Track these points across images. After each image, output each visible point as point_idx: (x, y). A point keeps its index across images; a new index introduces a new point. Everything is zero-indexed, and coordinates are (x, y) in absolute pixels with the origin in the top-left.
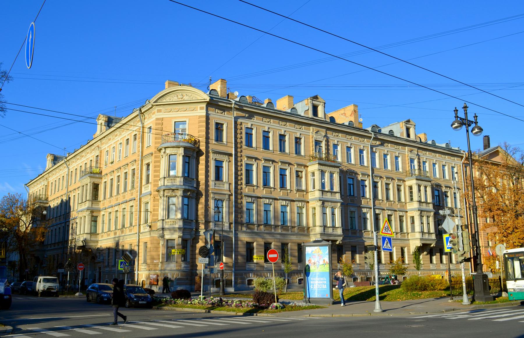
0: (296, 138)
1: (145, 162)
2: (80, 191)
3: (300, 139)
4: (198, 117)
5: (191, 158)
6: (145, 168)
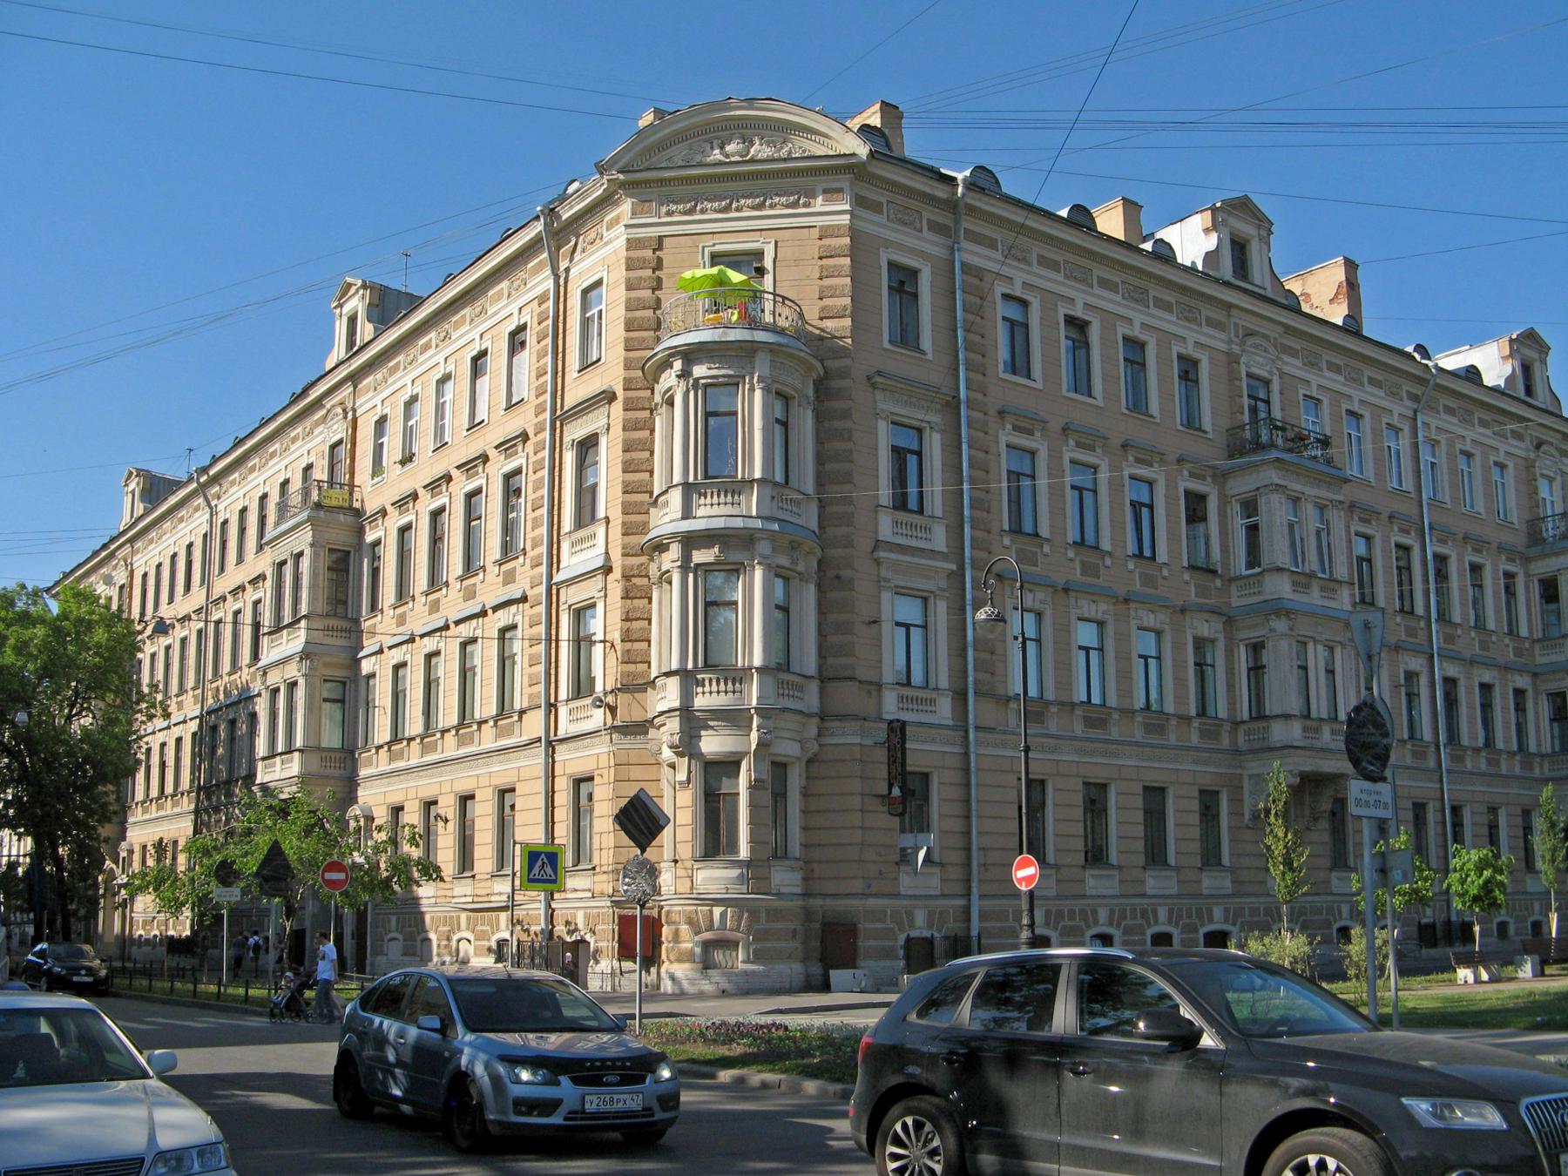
1: (576, 431)
2: (266, 592)
4: (815, 233)
5: (794, 404)
6: (569, 458)
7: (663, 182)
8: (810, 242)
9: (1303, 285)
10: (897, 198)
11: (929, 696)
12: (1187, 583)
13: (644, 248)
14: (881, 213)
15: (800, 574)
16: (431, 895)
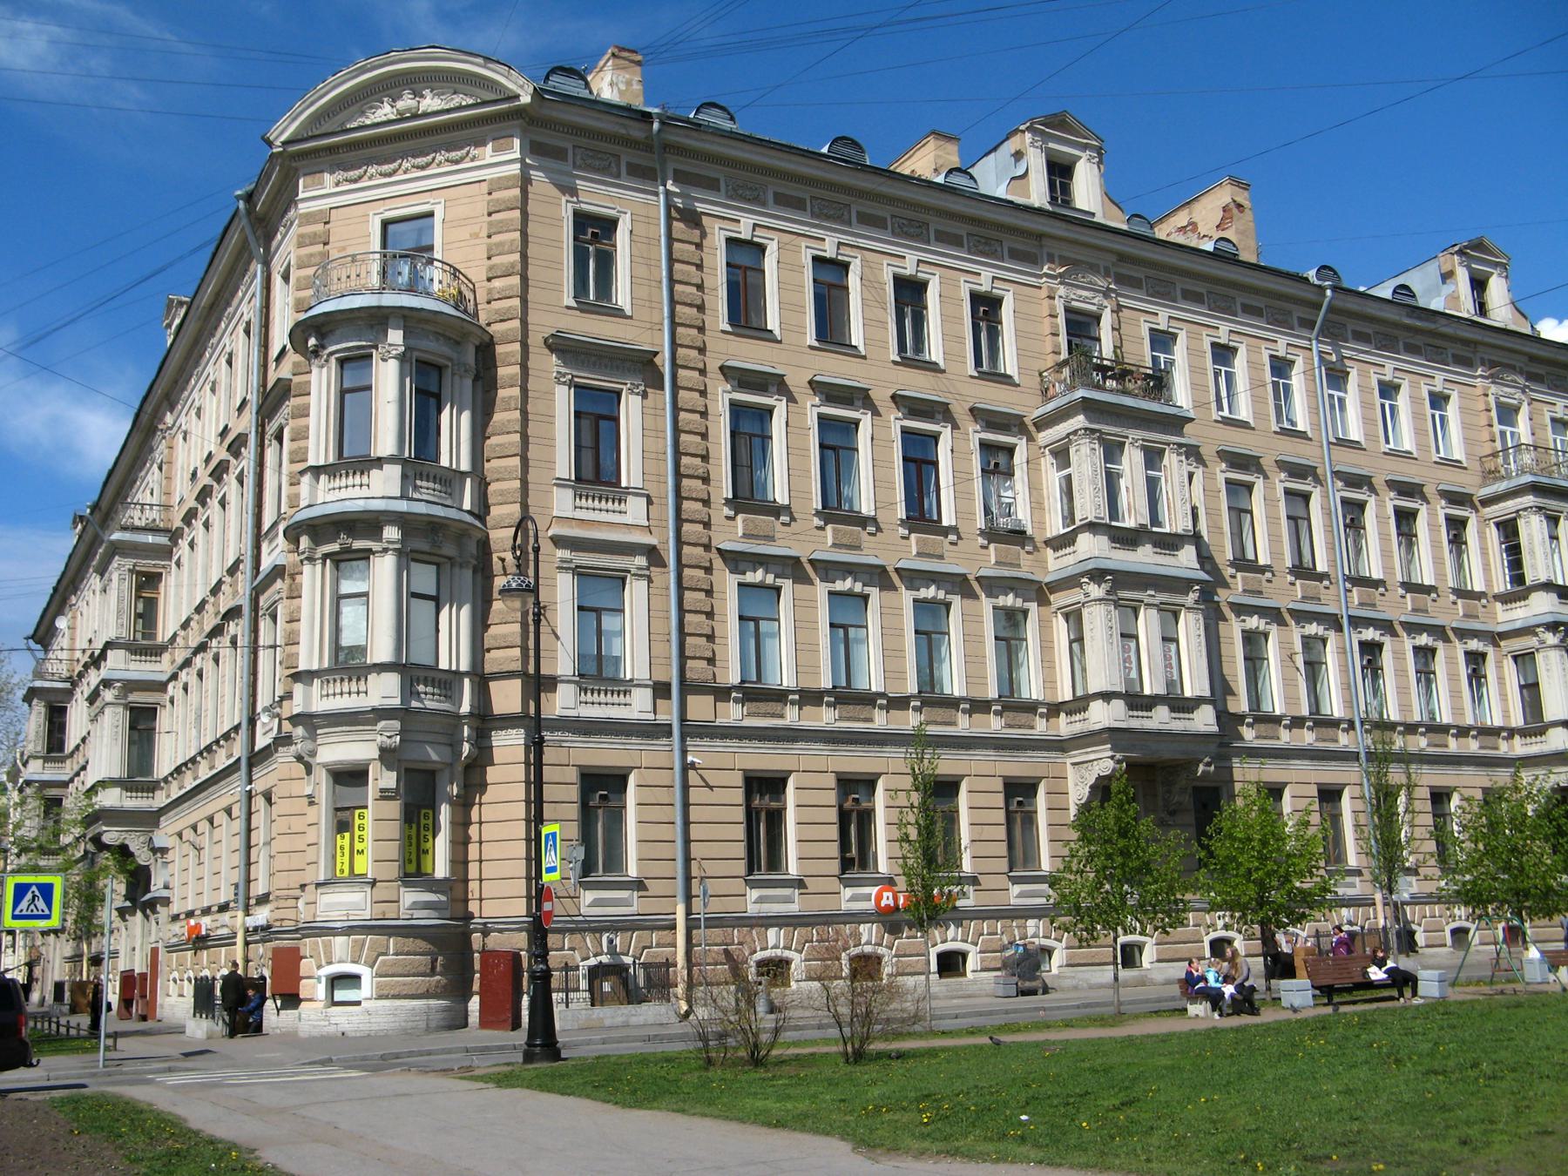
0: (977, 299)
3: (921, 287)
5: (448, 374)
9: (1190, 213)
10: (583, 141)
12: (1403, 597)
13: (315, 222)
14: (564, 159)
15: (450, 558)
16: (718, 940)
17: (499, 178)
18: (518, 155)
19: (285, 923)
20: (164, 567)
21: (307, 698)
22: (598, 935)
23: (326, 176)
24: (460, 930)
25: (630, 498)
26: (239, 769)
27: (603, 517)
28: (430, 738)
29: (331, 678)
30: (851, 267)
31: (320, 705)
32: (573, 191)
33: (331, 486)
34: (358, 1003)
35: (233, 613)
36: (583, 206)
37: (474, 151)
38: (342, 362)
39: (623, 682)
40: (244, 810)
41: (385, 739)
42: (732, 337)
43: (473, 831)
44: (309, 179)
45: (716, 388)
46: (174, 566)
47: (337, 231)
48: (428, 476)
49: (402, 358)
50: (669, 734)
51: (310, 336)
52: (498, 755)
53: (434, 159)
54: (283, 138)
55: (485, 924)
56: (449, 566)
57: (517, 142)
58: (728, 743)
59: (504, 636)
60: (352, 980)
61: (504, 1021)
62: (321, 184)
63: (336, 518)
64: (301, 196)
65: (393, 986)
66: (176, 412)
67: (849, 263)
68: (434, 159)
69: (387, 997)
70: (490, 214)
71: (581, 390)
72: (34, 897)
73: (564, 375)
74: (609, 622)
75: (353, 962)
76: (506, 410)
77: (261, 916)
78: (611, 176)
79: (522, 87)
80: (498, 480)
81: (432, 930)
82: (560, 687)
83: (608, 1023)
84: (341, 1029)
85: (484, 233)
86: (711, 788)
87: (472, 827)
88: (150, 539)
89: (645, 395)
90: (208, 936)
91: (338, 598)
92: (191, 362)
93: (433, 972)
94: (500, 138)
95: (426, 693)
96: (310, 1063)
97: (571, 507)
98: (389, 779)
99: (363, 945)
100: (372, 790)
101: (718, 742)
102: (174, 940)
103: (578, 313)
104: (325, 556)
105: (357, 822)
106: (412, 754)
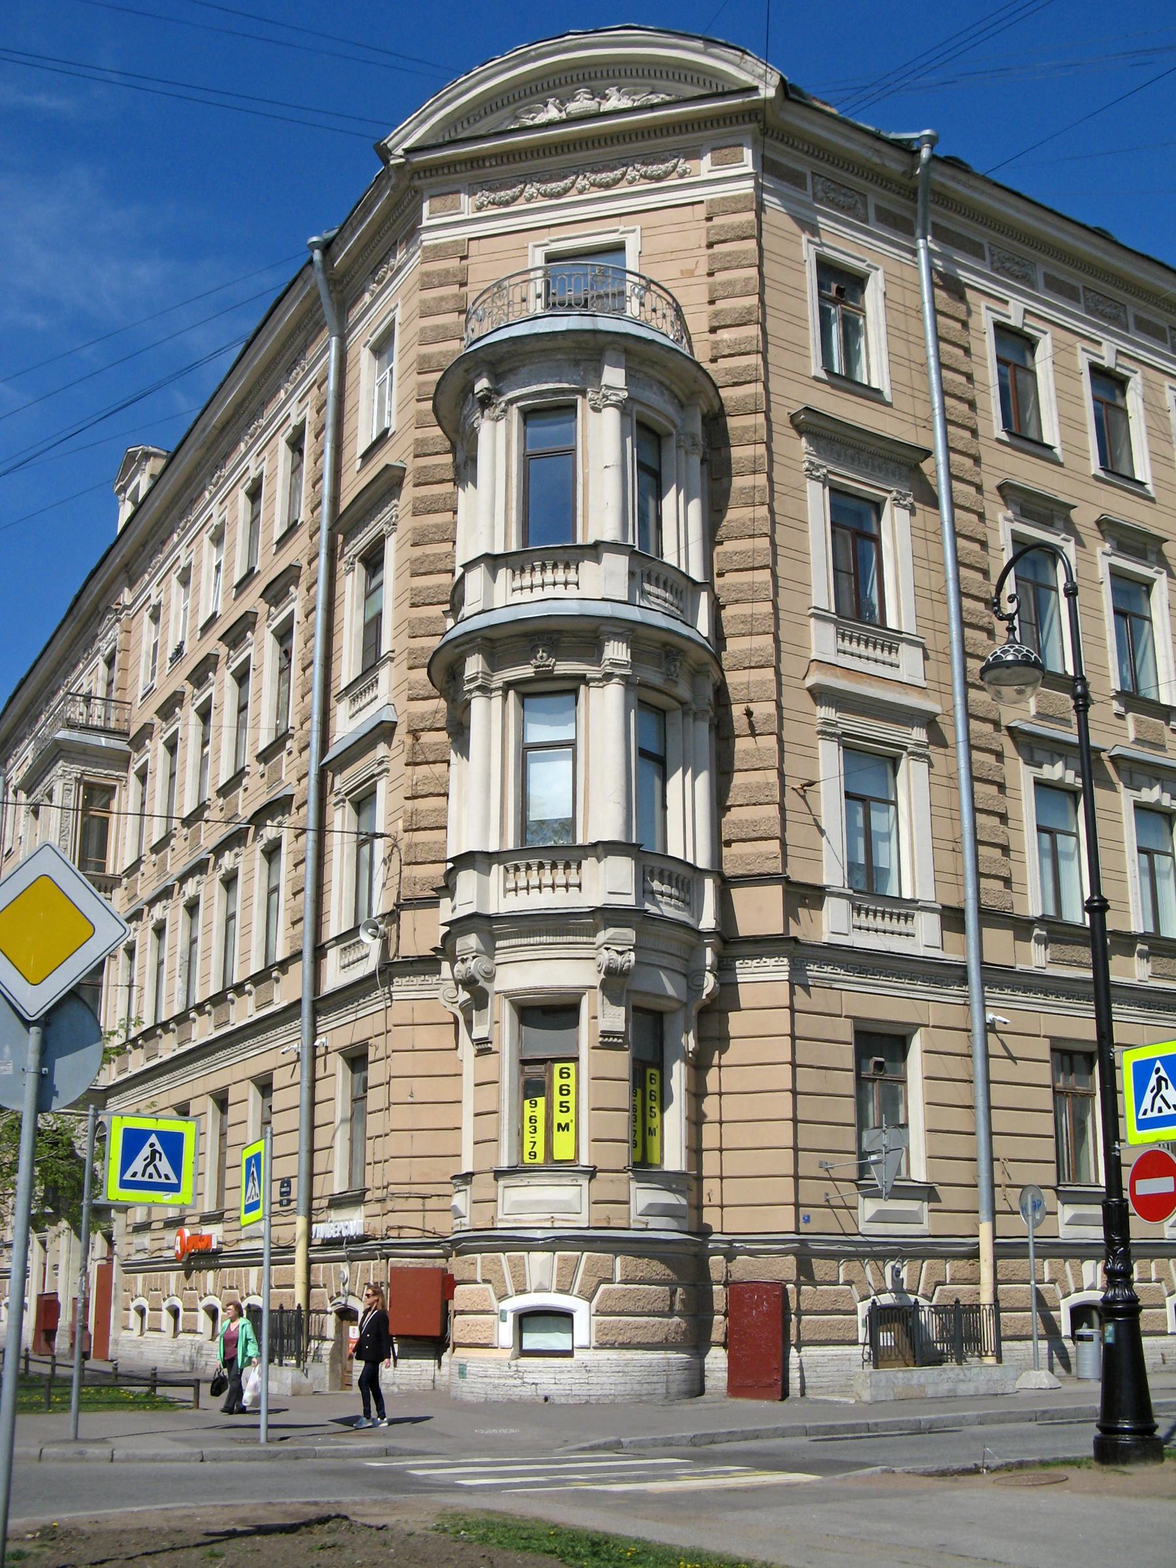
7: (475, 161)
8: (695, 225)
11: (903, 911)
15: (683, 703)
17: (723, 198)
18: (750, 169)
19: (405, 1233)
20: (118, 779)
21: (483, 892)
22: (880, 1263)
23: (464, 198)
24: (694, 1249)
25: (903, 647)
26: (298, 1016)
27: (872, 668)
28: (666, 961)
29: (522, 863)
30: (1131, 384)
31: (500, 904)
32: (814, 230)
33: (517, 584)
34: (568, 1354)
35: (279, 806)
36: (827, 251)
37: (683, 165)
38: (528, 415)
39: (899, 900)
40: (306, 1074)
41: (614, 955)
42: (1008, 450)
43: (710, 1106)
44: (437, 202)
45: (995, 514)
46: (133, 779)
47: (482, 273)
48: (657, 579)
49: (623, 408)
50: (964, 980)
51: (479, 376)
52: (746, 995)
53: (624, 175)
54: (406, 145)
55: (730, 1242)
56: (679, 713)
57: (748, 154)
58: (1031, 997)
59: (755, 823)
60: (562, 1318)
61: (770, 1386)
62: (456, 207)
63: (529, 627)
64: (425, 223)
65: (621, 1330)
66: (138, 588)
67: (1127, 379)
68: (624, 175)
69: (612, 1346)
70: (710, 245)
71: (837, 492)
72: (154, 1152)
73: (818, 467)
74: (879, 820)
75: (560, 1291)
76: (746, 505)
77: (352, 1222)
78: (856, 217)
79: (760, 77)
80: (737, 602)
81: (672, 1248)
82: (829, 902)
83: (930, 1391)
84: (543, 1391)
85: (703, 269)
86: (1014, 1059)
87: (707, 1100)
88: (103, 741)
89: (913, 512)
90: (219, 1251)
91: (526, 751)
92: (175, 512)
93: (671, 1313)
94: (723, 149)
95: (662, 894)
96: (583, 1449)
97: (833, 650)
98: (615, 1018)
99: (577, 1266)
100: (586, 1034)
101: (1020, 996)
102: (141, 1256)
103: (827, 388)
104: (509, 685)
105: (558, 1081)
106: (642, 984)
